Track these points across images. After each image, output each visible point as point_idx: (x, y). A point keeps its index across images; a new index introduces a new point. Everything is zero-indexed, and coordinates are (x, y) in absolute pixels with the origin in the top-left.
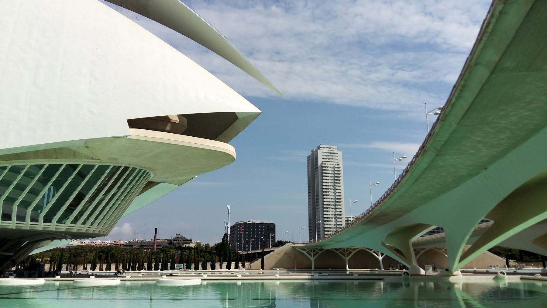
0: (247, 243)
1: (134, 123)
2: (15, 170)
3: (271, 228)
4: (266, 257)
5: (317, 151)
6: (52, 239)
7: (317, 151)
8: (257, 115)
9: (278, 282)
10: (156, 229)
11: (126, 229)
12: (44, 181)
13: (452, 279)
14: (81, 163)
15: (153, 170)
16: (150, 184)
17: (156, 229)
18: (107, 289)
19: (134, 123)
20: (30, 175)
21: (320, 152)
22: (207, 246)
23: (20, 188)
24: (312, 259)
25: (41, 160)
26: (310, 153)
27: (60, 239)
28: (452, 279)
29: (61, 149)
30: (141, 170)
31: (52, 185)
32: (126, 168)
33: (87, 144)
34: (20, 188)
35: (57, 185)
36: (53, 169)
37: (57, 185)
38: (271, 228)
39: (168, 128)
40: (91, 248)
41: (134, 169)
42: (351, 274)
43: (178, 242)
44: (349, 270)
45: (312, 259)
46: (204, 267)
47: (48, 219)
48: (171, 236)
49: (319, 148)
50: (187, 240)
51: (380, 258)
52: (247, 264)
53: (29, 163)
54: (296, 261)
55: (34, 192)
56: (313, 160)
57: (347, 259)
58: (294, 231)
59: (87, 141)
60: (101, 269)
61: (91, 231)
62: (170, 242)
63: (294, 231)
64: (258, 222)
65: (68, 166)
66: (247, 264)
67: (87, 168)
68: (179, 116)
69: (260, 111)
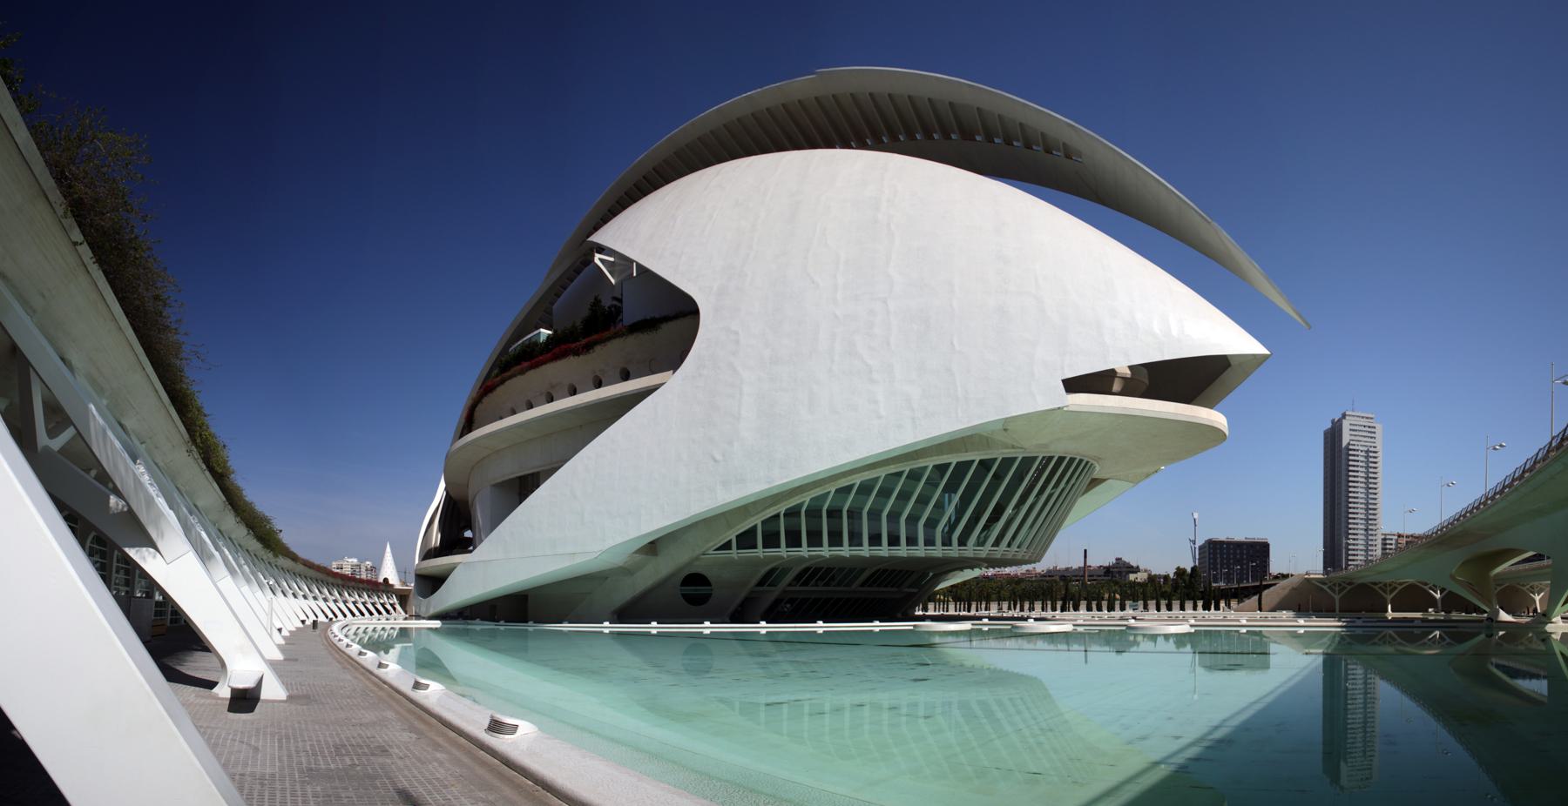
0: (1230, 572)
1: (1074, 385)
2: (915, 476)
3: (1260, 551)
4: (1265, 593)
5: (1340, 421)
6: (961, 569)
7: (1340, 421)
8: (1264, 358)
9: (1244, 630)
11: (1067, 550)
12: (932, 484)
13: (1549, 628)
14: (999, 454)
15: (1098, 459)
16: (1095, 482)
18: (884, 639)
19: (1074, 385)
20: (885, 493)
21: (1346, 424)
22: (1180, 572)
24: (1337, 597)
26: (1329, 425)
27: (972, 568)
28: (1549, 628)
32: (1061, 459)
33: (1007, 424)
35: (951, 488)
36: (963, 467)
37: (951, 488)
38: (1260, 551)
39: (1117, 387)
40: (1015, 581)
41: (1072, 460)
42: (1394, 620)
44: (1390, 614)
45: (1337, 597)
46: (1099, 609)
47: (962, 542)
48: (1108, 561)
49: (1344, 416)
51: (1438, 596)
52: (1234, 603)
53: (882, 473)
54: (1307, 599)
55: (923, 501)
56: (1333, 437)
57: (1389, 597)
58: (1298, 553)
59: (1006, 420)
60: (1000, 609)
61: (1019, 557)
62: (1107, 570)
63: (1298, 553)
64: (1223, 538)
65: (981, 462)
66: (1234, 603)
67: (1008, 462)
68: (1131, 367)
69: (1261, 350)
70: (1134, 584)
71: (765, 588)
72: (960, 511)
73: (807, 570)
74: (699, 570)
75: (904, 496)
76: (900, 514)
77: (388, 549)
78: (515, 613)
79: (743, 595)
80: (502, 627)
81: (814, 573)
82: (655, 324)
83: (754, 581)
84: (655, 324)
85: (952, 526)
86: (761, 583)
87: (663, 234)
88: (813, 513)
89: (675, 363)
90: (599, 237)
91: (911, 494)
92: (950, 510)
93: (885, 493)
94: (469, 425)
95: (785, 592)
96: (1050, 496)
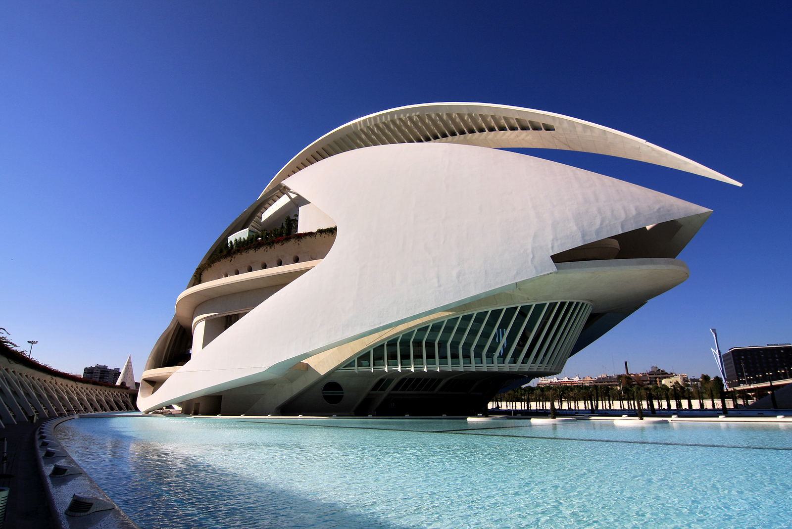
2: (467, 318)
10: (626, 362)
12: (491, 325)
17: (626, 362)
19: (557, 258)
20: (449, 329)
23: (473, 333)
25: (484, 307)
29: (499, 294)
30: (583, 304)
31: (498, 329)
32: (571, 304)
34: (473, 333)
35: (504, 326)
36: (496, 314)
37: (504, 326)
40: (549, 388)
43: (655, 376)
50: (667, 374)
55: (486, 335)
61: (542, 370)
70: (665, 388)
71: (377, 392)
72: (510, 340)
73: (404, 379)
74: (335, 380)
75: (461, 331)
76: (459, 343)
77: (704, 210)
78: (214, 404)
79: (363, 396)
80: (370, 421)
81: (408, 381)
82: (284, 239)
83: (371, 387)
84: (284, 239)
85: (506, 350)
86: (375, 388)
87: (320, 189)
88: (405, 343)
89: (322, 255)
90: (287, 182)
91: (465, 329)
92: (503, 341)
93: (449, 329)
94: (198, 279)
95: (389, 395)
96: (524, 338)
